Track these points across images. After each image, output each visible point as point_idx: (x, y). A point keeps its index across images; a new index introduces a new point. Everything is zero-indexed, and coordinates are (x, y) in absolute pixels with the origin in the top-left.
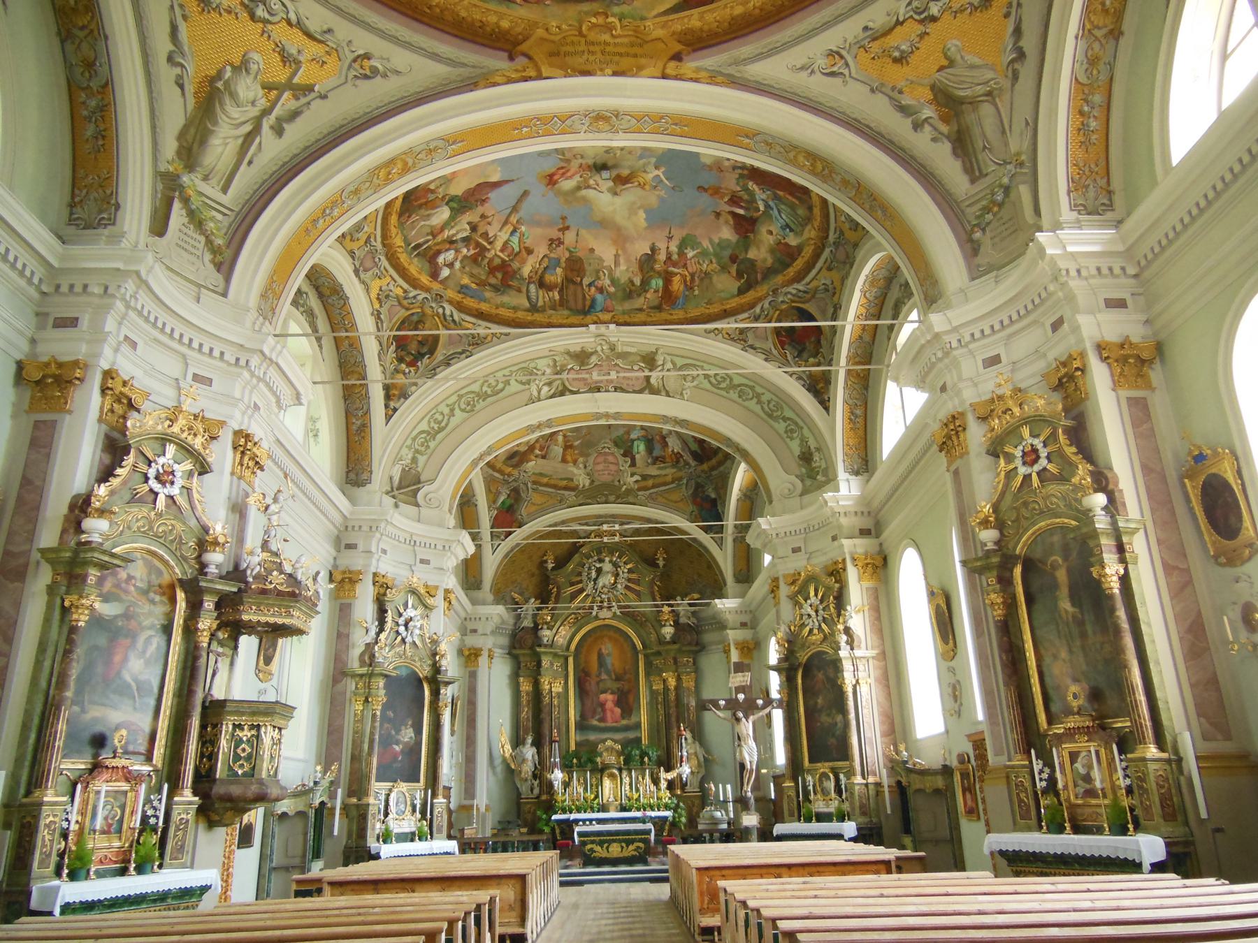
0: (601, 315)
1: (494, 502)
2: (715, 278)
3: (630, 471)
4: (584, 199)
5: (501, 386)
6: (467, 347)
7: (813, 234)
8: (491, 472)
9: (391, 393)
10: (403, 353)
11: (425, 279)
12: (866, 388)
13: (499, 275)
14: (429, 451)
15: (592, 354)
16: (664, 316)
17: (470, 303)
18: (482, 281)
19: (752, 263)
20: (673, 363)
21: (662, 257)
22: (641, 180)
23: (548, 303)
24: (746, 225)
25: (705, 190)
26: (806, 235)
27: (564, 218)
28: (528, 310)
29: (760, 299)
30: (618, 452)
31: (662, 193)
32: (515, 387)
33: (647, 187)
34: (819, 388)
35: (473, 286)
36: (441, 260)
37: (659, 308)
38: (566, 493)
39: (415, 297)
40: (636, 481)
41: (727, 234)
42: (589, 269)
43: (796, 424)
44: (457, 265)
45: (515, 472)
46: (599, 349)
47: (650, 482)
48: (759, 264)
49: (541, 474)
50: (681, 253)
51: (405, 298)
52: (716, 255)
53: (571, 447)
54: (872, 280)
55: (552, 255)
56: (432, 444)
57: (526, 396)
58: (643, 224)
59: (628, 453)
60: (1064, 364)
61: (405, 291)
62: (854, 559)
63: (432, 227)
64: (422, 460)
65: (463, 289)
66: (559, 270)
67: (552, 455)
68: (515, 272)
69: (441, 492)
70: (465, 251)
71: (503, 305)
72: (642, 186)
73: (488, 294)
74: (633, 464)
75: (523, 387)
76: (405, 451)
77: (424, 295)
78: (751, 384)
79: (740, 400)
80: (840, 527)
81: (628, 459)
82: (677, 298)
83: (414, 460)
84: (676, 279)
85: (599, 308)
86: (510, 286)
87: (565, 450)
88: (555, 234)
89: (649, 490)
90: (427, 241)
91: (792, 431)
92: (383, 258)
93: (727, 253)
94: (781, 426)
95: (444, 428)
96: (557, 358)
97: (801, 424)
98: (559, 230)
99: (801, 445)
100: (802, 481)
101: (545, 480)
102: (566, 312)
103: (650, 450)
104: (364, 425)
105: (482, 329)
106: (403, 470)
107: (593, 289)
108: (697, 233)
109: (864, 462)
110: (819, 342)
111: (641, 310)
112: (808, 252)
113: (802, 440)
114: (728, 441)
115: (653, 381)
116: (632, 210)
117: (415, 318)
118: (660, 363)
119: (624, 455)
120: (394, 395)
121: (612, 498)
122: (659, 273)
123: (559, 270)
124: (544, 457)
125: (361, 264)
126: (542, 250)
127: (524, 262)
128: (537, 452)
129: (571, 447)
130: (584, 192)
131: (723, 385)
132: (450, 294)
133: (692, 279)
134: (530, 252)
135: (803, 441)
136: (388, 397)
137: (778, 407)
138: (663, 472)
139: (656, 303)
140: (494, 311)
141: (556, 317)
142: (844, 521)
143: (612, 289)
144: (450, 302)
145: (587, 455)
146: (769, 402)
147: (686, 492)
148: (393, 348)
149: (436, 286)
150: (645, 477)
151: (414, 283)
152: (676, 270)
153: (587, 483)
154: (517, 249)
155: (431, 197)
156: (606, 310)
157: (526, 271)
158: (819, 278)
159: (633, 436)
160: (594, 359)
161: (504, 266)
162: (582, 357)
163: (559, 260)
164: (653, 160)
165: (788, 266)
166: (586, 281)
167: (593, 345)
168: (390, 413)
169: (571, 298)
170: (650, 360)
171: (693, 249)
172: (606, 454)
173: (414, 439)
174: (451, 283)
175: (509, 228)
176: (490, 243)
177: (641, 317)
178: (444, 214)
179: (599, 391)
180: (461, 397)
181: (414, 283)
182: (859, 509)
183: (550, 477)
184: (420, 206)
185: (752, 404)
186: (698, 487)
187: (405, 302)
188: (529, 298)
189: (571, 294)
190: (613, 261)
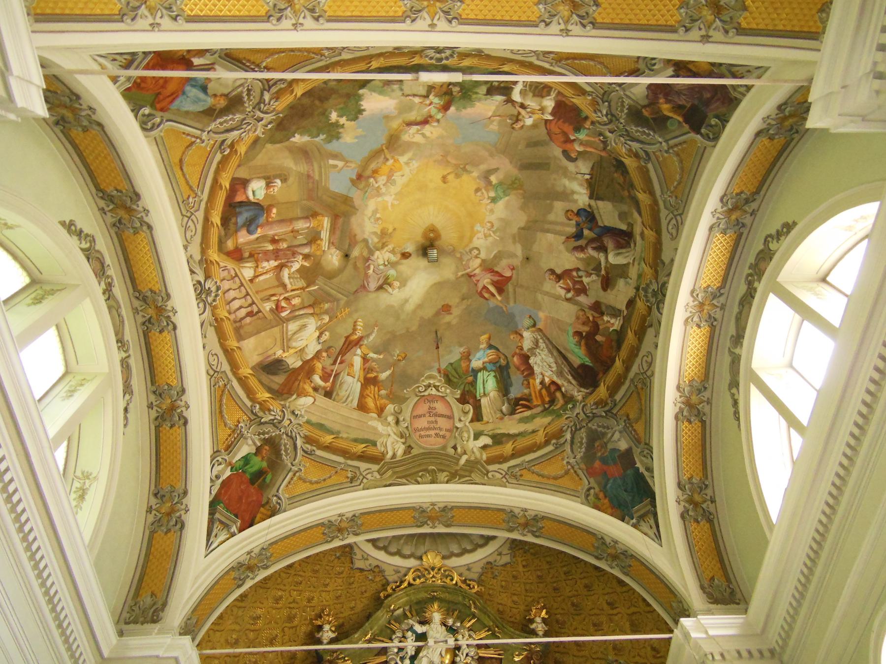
1: (229, 448)
3: (472, 428)
30: (452, 395)
38: (363, 466)
40: (485, 447)
45: (275, 406)
47: (508, 448)
49: (321, 427)
53: (374, 381)
59: (468, 397)
67: (343, 393)
74: (478, 417)
81: (469, 407)
87: (364, 387)
89: (506, 457)
101: (328, 439)
103: (504, 386)
119: (463, 400)
121: (443, 476)
124: (328, 394)
128: (317, 379)
129: (374, 381)
138: (529, 427)
145: (399, 400)
147: (572, 456)
150: (498, 439)
153: (400, 450)
159: (476, 363)
172: (432, 399)
183: (336, 434)
186: (594, 437)
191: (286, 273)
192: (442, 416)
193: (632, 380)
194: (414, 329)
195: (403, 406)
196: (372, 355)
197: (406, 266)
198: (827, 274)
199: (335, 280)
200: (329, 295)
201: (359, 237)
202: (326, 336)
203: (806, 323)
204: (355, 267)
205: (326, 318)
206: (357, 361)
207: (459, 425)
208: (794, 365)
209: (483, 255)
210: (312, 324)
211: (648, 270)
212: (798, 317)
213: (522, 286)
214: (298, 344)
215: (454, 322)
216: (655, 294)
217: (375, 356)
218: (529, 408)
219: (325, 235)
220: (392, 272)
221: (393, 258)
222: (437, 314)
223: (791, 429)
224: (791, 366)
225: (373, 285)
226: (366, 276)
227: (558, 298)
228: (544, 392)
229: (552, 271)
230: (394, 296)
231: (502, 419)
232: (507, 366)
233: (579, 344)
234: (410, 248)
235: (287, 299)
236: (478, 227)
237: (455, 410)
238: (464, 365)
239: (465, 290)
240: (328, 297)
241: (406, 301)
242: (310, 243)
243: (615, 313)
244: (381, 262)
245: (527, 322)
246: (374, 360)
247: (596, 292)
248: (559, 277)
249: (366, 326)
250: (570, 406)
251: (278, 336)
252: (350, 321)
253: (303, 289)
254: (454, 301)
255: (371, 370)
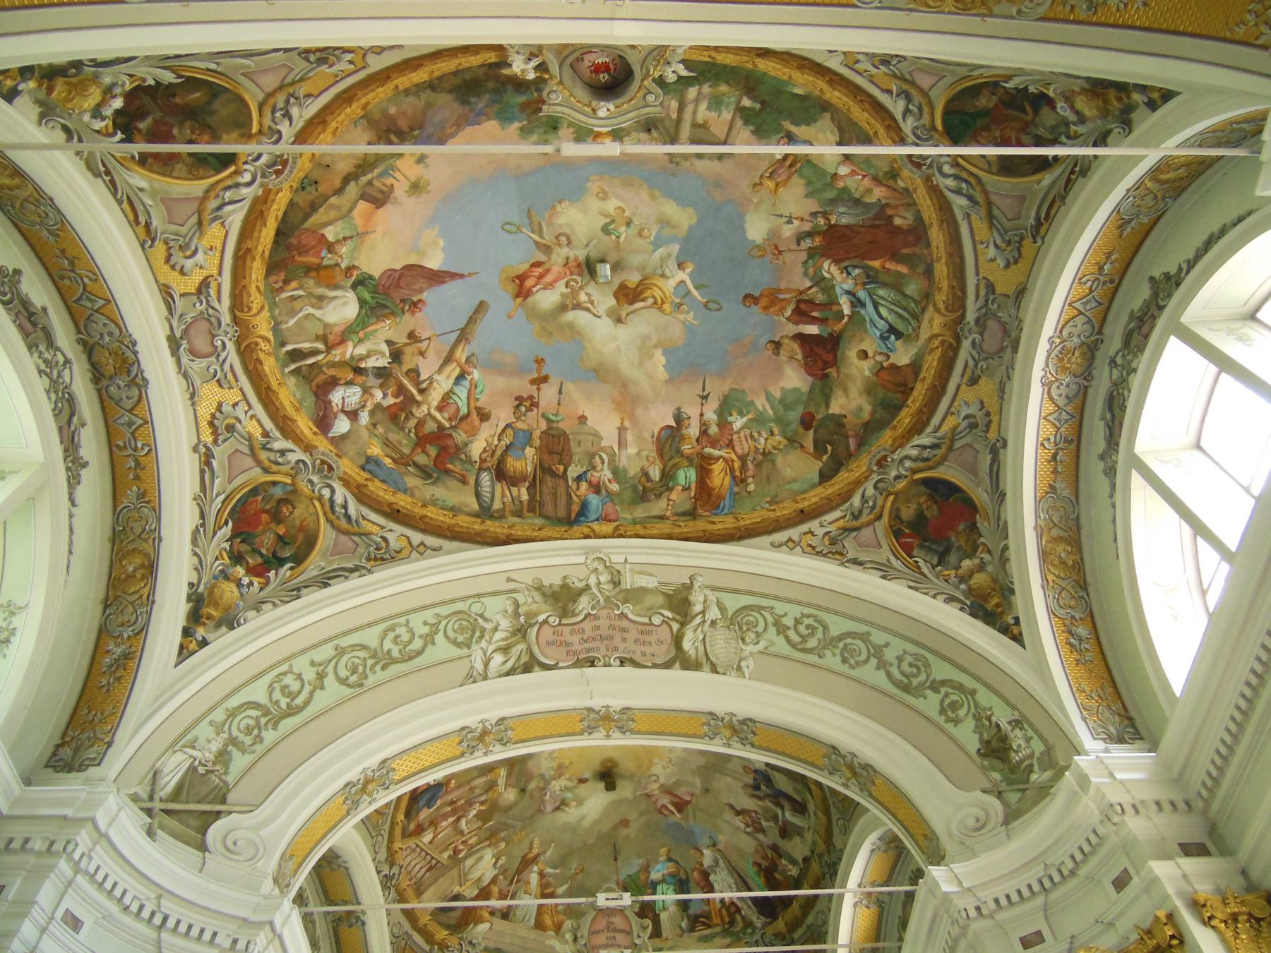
0: (596, 526)
2: (779, 460)
4: (571, 326)
5: (417, 644)
6: (364, 563)
7: (938, 321)
8: (407, 926)
9: (205, 611)
10: (244, 548)
11: (305, 425)
12: (1083, 585)
13: (433, 451)
14: (259, 748)
15: (581, 592)
16: (701, 525)
17: (377, 489)
18: (402, 455)
19: (838, 421)
20: (722, 608)
21: (693, 431)
22: (657, 293)
23: (510, 507)
24: (821, 355)
25: (756, 300)
26: (925, 333)
27: (540, 362)
28: (476, 515)
29: (858, 483)
31: (690, 317)
32: (442, 648)
33: (667, 307)
34: (994, 607)
35: (388, 461)
36: (336, 397)
37: (692, 514)
39: (283, 452)
41: (794, 379)
42: (577, 451)
43: (960, 688)
44: (364, 418)
46: (593, 581)
48: (850, 420)
50: (723, 424)
51: (264, 448)
52: (778, 420)
54: (1061, 357)
55: (520, 425)
56: (269, 736)
57: (463, 667)
58: (662, 374)
60: (1149, 932)
61: (266, 434)
62: (1197, 906)
63: (326, 326)
64: (239, 761)
65: (369, 464)
66: (530, 452)
68: (458, 449)
69: (264, 833)
70: (378, 394)
71: (434, 502)
72: (658, 305)
73: (412, 481)
75: (459, 652)
76: (204, 731)
77: (297, 455)
78: (862, 628)
79: (845, 669)
80: (1128, 846)
81: (648, 922)
82: (720, 497)
83: (223, 757)
84: (718, 467)
85: (593, 516)
86: (448, 472)
88: (526, 389)
90: (315, 352)
91: (954, 706)
92: (230, 346)
93: (795, 415)
94: (931, 703)
95: (299, 709)
96: (520, 598)
97: (969, 683)
98: (533, 382)
99: (978, 729)
100: (999, 795)
102: (539, 521)
104: (127, 656)
105: (396, 534)
106: (192, 769)
107: (584, 485)
108: (745, 385)
109: (1127, 708)
110: (973, 527)
111: (661, 517)
112: (931, 364)
113: (977, 718)
114: (835, 757)
115: (687, 645)
116: (645, 353)
117: (278, 492)
118: (698, 608)
120: (205, 614)
122: (689, 458)
123: (530, 452)
125: (185, 332)
126: (503, 415)
127: (473, 433)
130: (571, 316)
131: (812, 643)
132: (346, 466)
133: (744, 467)
134: (484, 416)
135: (982, 718)
136: (195, 616)
137: (920, 664)
139: (687, 506)
140: (418, 511)
141: (521, 526)
142: (1136, 825)
143: (615, 487)
144: (346, 483)
146: (900, 659)
148: (227, 531)
149: (322, 445)
151: (285, 426)
152: (716, 452)
154: (464, 410)
155: (329, 259)
156: (605, 518)
157: (476, 449)
158: (960, 402)
159: (655, 875)
160: (584, 604)
161: (440, 436)
162: (563, 597)
163: (529, 434)
164: (675, 248)
165: (898, 408)
166: (573, 472)
167: (583, 573)
168: (190, 643)
169: (548, 500)
170: (679, 602)
171: (741, 414)
173: (232, 714)
174: (349, 447)
175: (453, 370)
176: (421, 391)
177: (666, 527)
178: (343, 308)
179: (592, 664)
180: (340, 652)
181: (285, 426)
182: (1164, 795)
184: (309, 269)
185: (870, 673)
187: (263, 455)
188: (478, 495)
189: (548, 489)
190: (616, 437)
191: (463, 822)
192: (620, 931)
193: (809, 927)
194: (592, 841)
195: (581, 922)
196: (549, 870)
197: (582, 790)
198: (1257, 310)
199: (512, 812)
200: (505, 824)
201: (536, 773)
202: (502, 861)
203: (1224, 376)
204: (532, 797)
205: (503, 845)
206: (534, 878)
207: (637, 941)
208: (1202, 444)
209: (662, 780)
210: (488, 856)
211: (820, 842)
212: (1213, 369)
213: (701, 810)
214: (475, 875)
215: (633, 835)
216: (828, 865)
217: (551, 871)
218: (709, 926)
219: (501, 782)
220: (569, 795)
221: (569, 784)
222: (615, 828)
223: (1199, 538)
224: (1198, 446)
225: (549, 808)
226: (543, 802)
227: (739, 828)
228: (724, 912)
229: (732, 807)
230: (571, 814)
231: (681, 936)
232: (687, 879)
233: (758, 873)
234: (587, 775)
235: (464, 842)
236: (656, 760)
237: (633, 923)
238: (643, 876)
239: (643, 807)
240: (504, 826)
241: (583, 817)
242: (487, 791)
243: (793, 862)
244: (557, 788)
245: (707, 841)
246: (550, 875)
247: (773, 836)
248: (738, 813)
249: (542, 844)
250: (749, 930)
251: (456, 877)
252: (527, 841)
253: (480, 828)
254: (633, 816)
255: (548, 885)
